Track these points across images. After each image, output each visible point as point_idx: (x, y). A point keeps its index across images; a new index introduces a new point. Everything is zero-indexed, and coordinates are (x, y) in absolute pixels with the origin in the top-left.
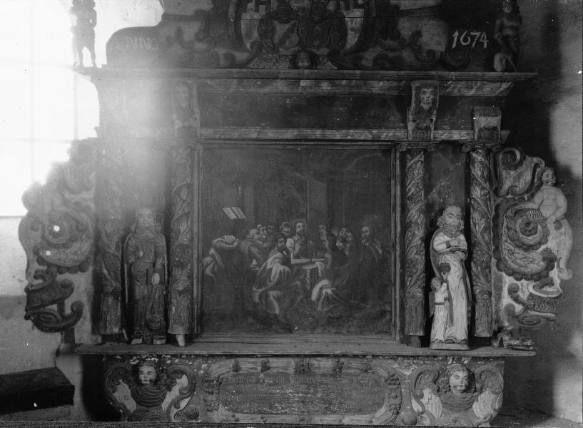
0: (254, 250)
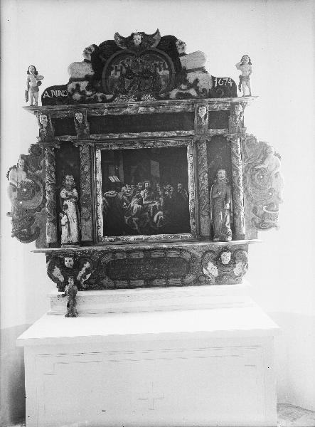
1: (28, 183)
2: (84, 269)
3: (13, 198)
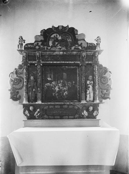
0: (53, 86)
1: (17, 79)
2: (37, 111)
3: (11, 84)
